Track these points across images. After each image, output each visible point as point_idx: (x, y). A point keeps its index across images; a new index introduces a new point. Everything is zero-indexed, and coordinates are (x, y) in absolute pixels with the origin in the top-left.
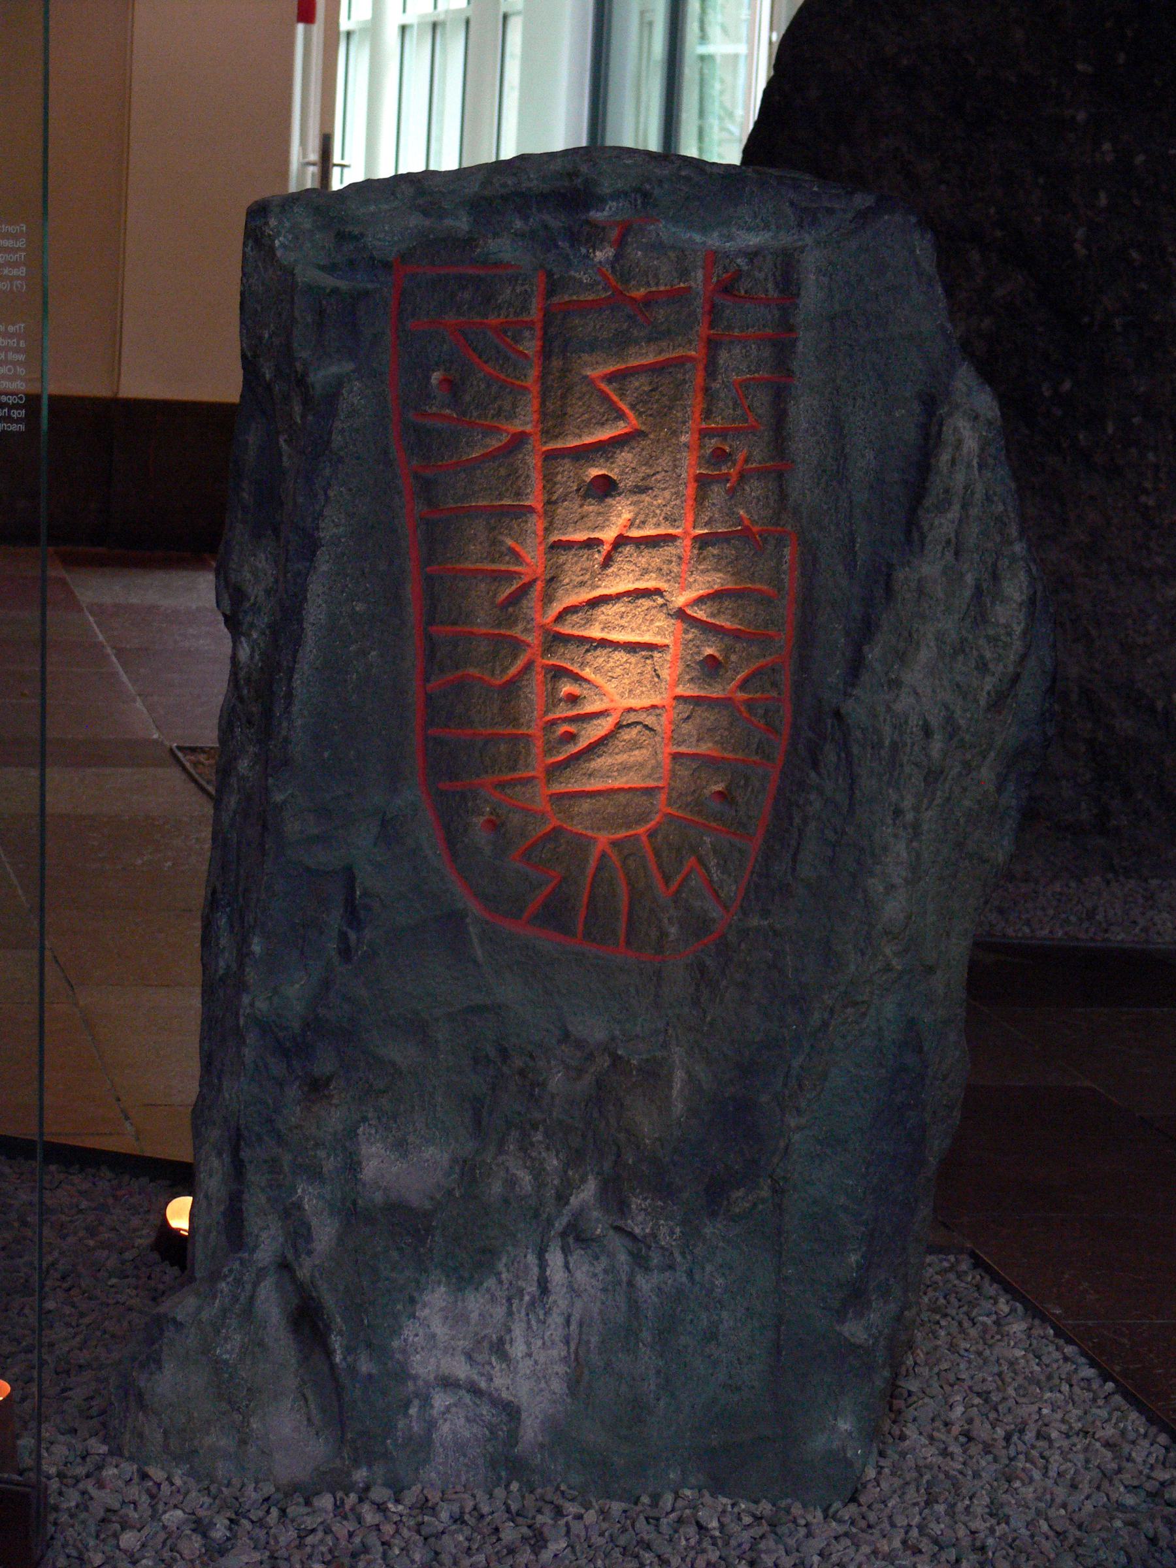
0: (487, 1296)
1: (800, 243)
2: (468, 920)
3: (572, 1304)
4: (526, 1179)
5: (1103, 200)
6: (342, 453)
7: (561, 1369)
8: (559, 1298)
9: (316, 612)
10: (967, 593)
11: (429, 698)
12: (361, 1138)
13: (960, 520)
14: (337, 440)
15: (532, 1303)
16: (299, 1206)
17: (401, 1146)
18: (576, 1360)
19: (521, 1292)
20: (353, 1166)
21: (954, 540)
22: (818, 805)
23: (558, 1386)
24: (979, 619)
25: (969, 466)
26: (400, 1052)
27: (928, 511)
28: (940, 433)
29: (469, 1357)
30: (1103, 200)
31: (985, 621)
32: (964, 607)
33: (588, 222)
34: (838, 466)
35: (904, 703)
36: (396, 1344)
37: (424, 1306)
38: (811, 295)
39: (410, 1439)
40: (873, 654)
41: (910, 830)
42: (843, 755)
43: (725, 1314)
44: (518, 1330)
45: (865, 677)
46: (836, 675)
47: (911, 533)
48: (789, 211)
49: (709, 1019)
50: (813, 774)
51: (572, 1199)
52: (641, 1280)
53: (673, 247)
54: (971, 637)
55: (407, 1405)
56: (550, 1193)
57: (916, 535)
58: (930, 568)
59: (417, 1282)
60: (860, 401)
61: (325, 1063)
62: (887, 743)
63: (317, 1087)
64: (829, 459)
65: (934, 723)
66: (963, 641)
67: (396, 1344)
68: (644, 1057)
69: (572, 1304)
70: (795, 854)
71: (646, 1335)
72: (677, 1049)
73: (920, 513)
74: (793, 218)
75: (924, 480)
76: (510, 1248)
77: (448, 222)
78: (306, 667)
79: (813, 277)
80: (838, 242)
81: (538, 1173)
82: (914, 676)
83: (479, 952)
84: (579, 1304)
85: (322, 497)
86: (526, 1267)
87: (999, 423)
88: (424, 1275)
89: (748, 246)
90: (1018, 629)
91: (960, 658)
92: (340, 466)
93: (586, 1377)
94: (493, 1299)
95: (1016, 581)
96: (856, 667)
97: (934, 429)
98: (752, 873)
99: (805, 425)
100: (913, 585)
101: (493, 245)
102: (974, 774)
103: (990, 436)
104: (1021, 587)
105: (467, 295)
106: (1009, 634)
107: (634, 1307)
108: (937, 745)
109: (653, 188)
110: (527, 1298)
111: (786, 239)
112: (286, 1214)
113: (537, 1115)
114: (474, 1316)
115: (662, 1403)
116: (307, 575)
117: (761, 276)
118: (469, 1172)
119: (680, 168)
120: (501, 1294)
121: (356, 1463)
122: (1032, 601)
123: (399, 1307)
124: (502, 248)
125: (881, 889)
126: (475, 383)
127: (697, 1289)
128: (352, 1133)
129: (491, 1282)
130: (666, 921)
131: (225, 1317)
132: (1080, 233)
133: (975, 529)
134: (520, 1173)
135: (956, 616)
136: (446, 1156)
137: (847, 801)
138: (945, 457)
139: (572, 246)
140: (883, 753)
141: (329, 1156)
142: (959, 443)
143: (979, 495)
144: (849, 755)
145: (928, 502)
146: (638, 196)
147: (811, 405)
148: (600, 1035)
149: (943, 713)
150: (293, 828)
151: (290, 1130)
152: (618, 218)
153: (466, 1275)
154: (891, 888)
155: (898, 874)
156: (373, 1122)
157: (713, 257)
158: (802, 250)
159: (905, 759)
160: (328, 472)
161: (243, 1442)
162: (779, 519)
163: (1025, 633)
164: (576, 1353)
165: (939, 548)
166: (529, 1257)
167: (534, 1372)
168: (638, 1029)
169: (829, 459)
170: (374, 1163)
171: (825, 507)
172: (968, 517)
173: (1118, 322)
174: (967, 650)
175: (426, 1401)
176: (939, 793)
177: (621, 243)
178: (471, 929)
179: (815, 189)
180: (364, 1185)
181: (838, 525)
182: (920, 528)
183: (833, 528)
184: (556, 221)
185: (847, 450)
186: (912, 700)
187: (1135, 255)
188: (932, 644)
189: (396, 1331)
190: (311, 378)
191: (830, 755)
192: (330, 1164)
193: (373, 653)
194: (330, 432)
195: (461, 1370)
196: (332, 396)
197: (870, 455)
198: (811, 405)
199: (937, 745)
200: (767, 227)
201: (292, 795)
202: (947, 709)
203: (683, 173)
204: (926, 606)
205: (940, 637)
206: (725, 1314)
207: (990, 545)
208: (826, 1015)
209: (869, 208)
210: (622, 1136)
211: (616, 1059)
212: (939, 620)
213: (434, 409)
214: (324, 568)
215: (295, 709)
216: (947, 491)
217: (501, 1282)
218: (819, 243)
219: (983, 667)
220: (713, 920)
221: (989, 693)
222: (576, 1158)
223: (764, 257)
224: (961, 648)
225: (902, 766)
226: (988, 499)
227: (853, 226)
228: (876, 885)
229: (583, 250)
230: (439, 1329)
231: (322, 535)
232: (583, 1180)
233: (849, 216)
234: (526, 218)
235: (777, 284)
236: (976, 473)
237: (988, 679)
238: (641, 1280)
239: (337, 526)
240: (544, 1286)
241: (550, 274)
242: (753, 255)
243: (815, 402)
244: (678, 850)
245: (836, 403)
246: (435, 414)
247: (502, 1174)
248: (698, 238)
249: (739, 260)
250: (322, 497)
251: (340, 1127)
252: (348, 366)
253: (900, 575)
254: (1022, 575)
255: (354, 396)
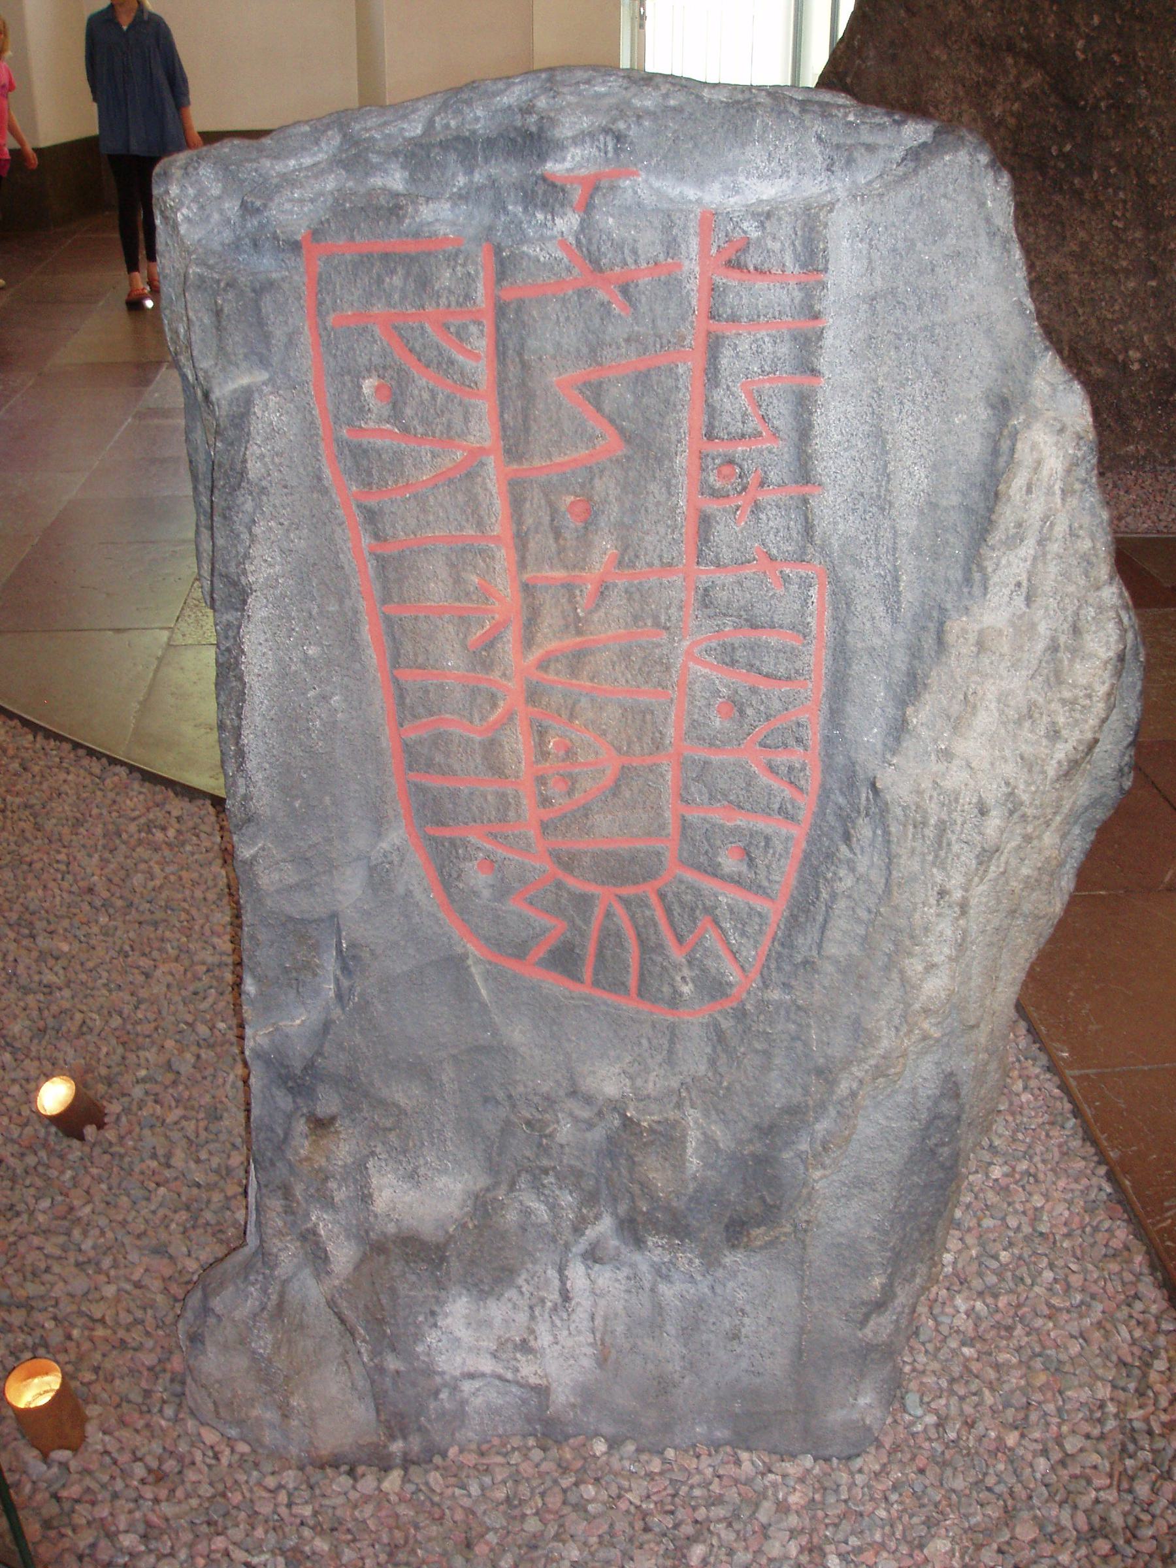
0: (510, 1305)
1: (829, 197)
2: (470, 962)
3: (595, 1304)
4: (541, 1211)
5: (1096, 20)
6: (264, 483)
7: (589, 1351)
8: (582, 1301)
9: (258, 661)
10: (1040, 646)
11: (407, 748)
12: (372, 1171)
13: (1035, 558)
14: (254, 469)
15: (555, 1309)
16: (314, 1232)
17: (413, 1176)
18: (603, 1344)
19: (542, 1301)
20: (366, 1198)
21: (1025, 583)
22: (849, 882)
23: (586, 1362)
24: (1052, 679)
25: (1050, 492)
26: (404, 1094)
27: (993, 548)
28: (1013, 450)
29: (494, 1355)
30: (1096, 20)
31: (1060, 681)
32: (1035, 662)
33: (544, 179)
34: (879, 487)
35: (955, 778)
36: (420, 1349)
37: (446, 1315)
38: (846, 269)
39: (444, 1414)
40: (919, 717)
41: (957, 909)
42: (879, 832)
43: (746, 1320)
44: (543, 1329)
45: (908, 743)
46: (873, 735)
47: (973, 572)
48: (816, 149)
49: (725, 1084)
50: (843, 848)
51: (587, 1232)
52: (663, 1288)
53: (657, 210)
54: (1041, 700)
55: (436, 1393)
56: (566, 1225)
57: (977, 576)
58: (996, 611)
59: (437, 1298)
60: (908, 405)
61: (328, 1102)
62: (932, 822)
63: (321, 1125)
64: (867, 479)
65: (990, 800)
66: (1032, 706)
67: (420, 1349)
68: (656, 1118)
69: (595, 1304)
70: (823, 929)
71: (669, 1328)
72: (691, 1111)
73: (984, 550)
74: (820, 159)
75: (991, 510)
76: (530, 1266)
77: (377, 181)
78: (258, 719)
79: (845, 243)
80: (881, 195)
81: (553, 1207)
82: (970, 746)
83: (484, 992)
84: (602, 1303)
85: (245, 536)
86: (547, 1281)
87: (1091, 436)
88: (443, 1293)
89: (760, 201)
90: (1102, 690)
91: (1027, 724)
92: (264, 498)
93: (613, 1355)
94: (515, 1307)
95: (1101, 634)
96: (899, 729)
97: (1005, 445)
98: (774, 939)
99: (837, 438)
100: (972, 638)
101: (426, 212)
102: (1035, 842)
103: (1079, 454)
104: (1108, 642)
105: (397, 280)
106: (1089, 696)
107: (659, 1308)
108: (994, 822)
109: (629, 127)
110: (549, 1304)
111: (813, 188)
112: (303, 1237)
113: (545, 1162)
114: (498, 1322)
115: (686, 1381)
116: (239, 627)
117: (777, 246)
118: (483, 1207)
119: (666, 96)
120: (523, 1303)
121: (392, 1437)
122: (1121, 658)
123: (421, 1318)
124: (438, 215)
125: (920, 968)
126: (416, 392)
127: (719, 1299)
128: (361, 1166)
129: (512, 1293)
130: (678, 979)
131: (255, 1321)
132: (1080, 44)
133: (1053, 569)
134: (534, 1205)
135: (1024, 673)
136: (459, 1186)
137: (883, 881)
138: (1019, 482)
139: (525, 209)
140: (927, 832)
141: (340, 1187)
142: (1038, 464)
143: (1061, 529)
144: (887, 833)
145: (996, 537)
146: (609, 138)
147: (845, 413)
148: (611, 1089)
149: (1005, 789)
150: (267, 879)
151: (300, 1161)
152: (583, 172)
153: (487, 1288)
154: (931, 967)
155: (942, 953)
156: (383, 1156)
157: (710, 220)
158: (831, 206)
159: (954, 838)
160: (249, 506)
161: (285, 1416)
162: (804, 553)
163: (1109, 694)
164: (602, 1340)
165: (1007, 591)
166: (549, 1272)
167: (561, 1355)
168: (651, 1085)
169: (867, 479)
170: (387, 1194)
171: (862, 538)
172: (1044, 555)
173: (1102, 104)
174: (1037, 715)
175: (455, 1389)
176: (993, 868)
177: (587, 207)
178: (473, 969)
179: (851, 118)
180: (376, 1216)
181: (878, 558)
182: (982, 569)
183: (871, 563)
184: (507, 171)
185: (890, 468)
186: (965, 775)
187: (1116, 58)
188: (993, 706)
189: (418, 1337)
190: (215, 395)
191: (864, 830)
192: (341, 1194)
193: (336, 698)
194: (244, 461)
195: (487, 1365)
196: (241, 417)
197: (920, 472)
198: (845, 413)
199: (994, 822)
200: (785, 173)
201: (263, 849)
202: (1007, 784)
203: (672, 103)
204: (987, 661)
205: (1003, 699)
206: (746, 1320)
207: (1071, 589)
208: (855, 1086)
209: (924, 144)
210: (636, 1188)
211: (627, 1123)
212: (1001, 678)
213: (372, 425)
214: (264, 613)
215: (251, 764)
216: (1019, 525)
217: (522, 1293)
218: (855, 197)
219: (1054, 734)
220: (730, 984)
221: (1059, 762)
222: (590, 1198)
223: (779, 219)
224: (1030, 713)
225: (949, 844)
226: (1073, 534)
227: (902, 169)
228: (914, 966)
229: (540, 216)
230: (463, 1333)
231: (251, 579)
232: (598, 1217)
233: (897, 155)
234: (470, 171)
235: (797, 258)
236: (1059, 501)
237: (1060, 746)
238: (663, 1288)
239: (270, 565)
240: (566, 1296)
241: (498, 249)
242: (765, 216)
243: (850, 408)
244: (692, 909)
245: (877, 410)
246: (374, 430)
247: (516, 1205)
248: (691, 193)
249: (745, 225)
250: (245, 536)
251: (350, 1160)
252: (263, 376)
253: (954, 627)
254: (1111, 626)
255: (272, 415)
